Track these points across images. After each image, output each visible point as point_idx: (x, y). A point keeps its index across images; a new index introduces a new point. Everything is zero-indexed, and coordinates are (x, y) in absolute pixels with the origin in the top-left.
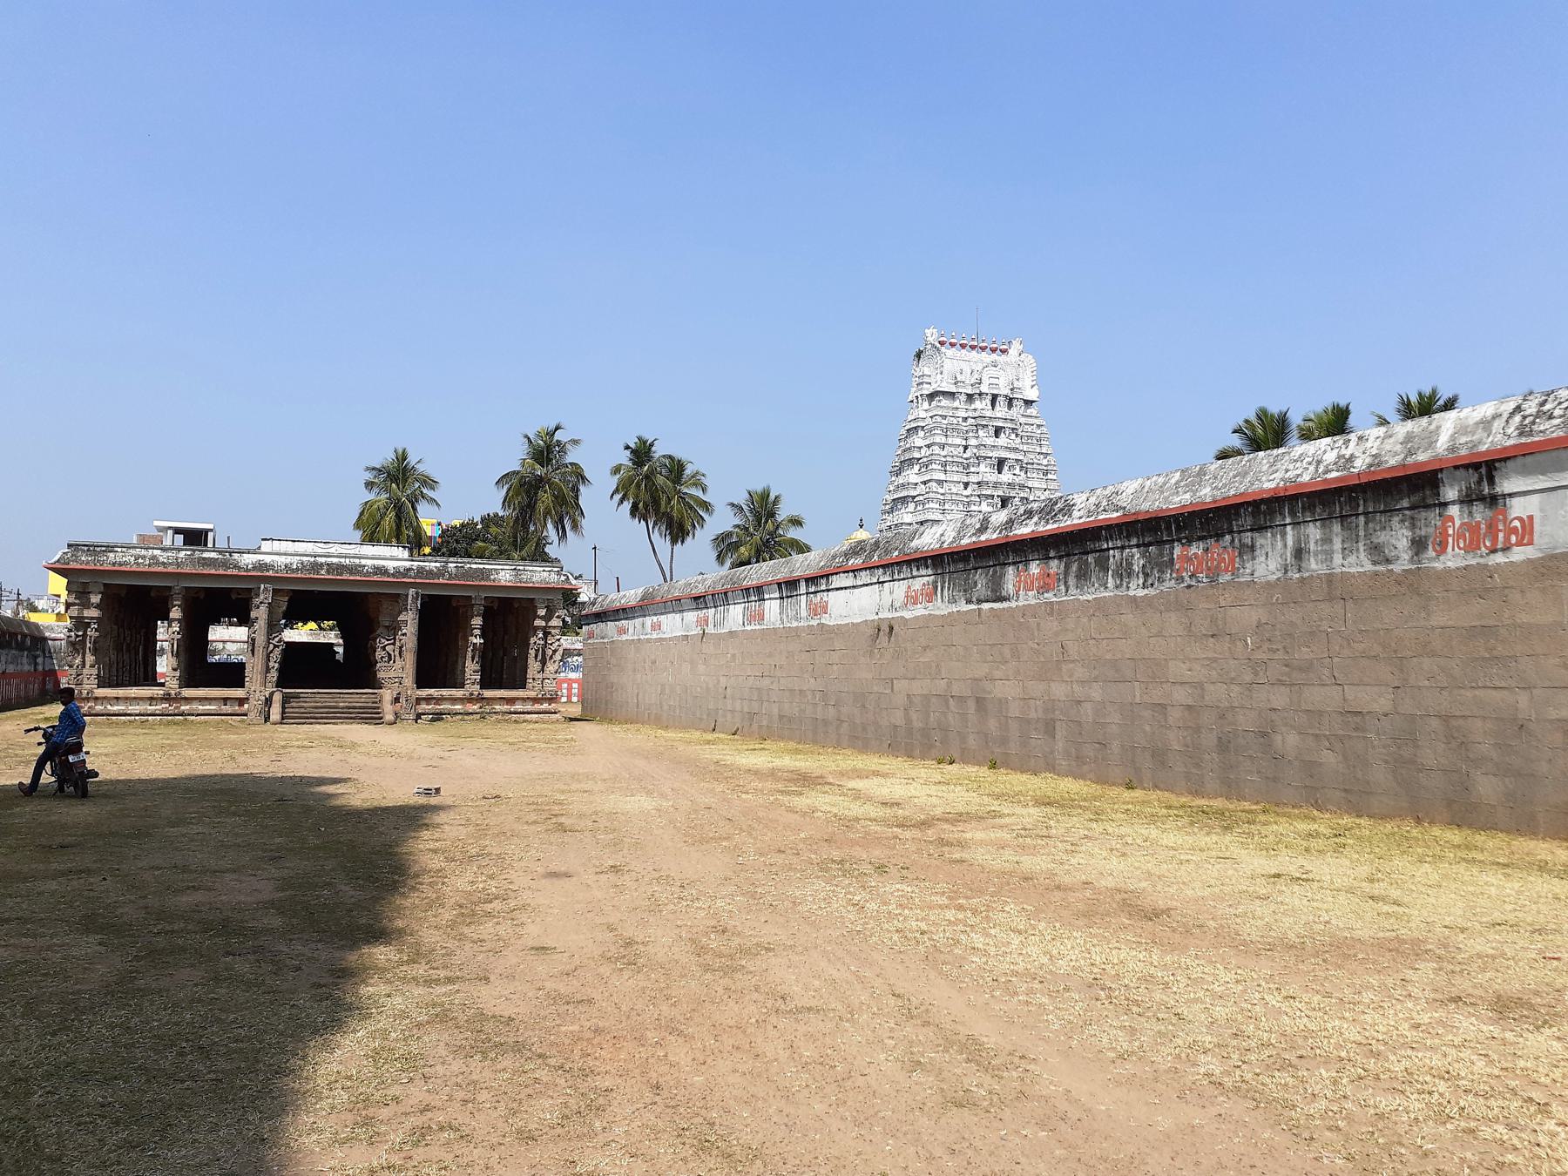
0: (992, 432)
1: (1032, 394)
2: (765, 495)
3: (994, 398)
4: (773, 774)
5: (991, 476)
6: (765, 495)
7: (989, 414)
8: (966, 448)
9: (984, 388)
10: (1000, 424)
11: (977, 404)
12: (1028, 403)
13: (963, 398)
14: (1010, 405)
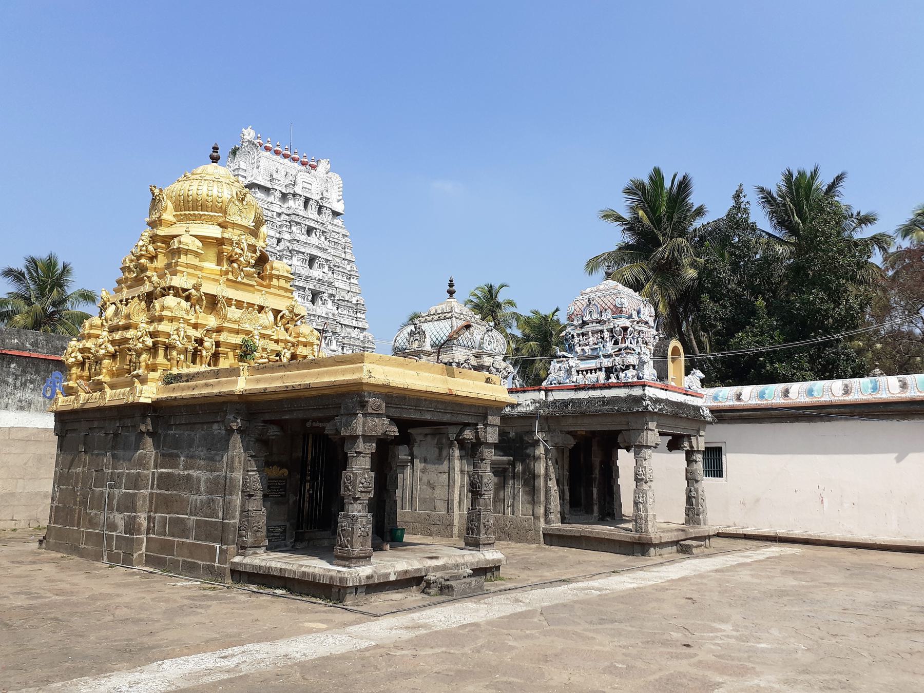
0: (304, 230)
1: (339, 207)
2: (50, 264)
3: (307, 201)
6: (50, 264)
7: (301, 213)
8: (279, 241)
9: (298, 190)
10: (312, 224)
11: (291, 203)
12: (336, 214)
13: (278, 195)
14: (320, 212)
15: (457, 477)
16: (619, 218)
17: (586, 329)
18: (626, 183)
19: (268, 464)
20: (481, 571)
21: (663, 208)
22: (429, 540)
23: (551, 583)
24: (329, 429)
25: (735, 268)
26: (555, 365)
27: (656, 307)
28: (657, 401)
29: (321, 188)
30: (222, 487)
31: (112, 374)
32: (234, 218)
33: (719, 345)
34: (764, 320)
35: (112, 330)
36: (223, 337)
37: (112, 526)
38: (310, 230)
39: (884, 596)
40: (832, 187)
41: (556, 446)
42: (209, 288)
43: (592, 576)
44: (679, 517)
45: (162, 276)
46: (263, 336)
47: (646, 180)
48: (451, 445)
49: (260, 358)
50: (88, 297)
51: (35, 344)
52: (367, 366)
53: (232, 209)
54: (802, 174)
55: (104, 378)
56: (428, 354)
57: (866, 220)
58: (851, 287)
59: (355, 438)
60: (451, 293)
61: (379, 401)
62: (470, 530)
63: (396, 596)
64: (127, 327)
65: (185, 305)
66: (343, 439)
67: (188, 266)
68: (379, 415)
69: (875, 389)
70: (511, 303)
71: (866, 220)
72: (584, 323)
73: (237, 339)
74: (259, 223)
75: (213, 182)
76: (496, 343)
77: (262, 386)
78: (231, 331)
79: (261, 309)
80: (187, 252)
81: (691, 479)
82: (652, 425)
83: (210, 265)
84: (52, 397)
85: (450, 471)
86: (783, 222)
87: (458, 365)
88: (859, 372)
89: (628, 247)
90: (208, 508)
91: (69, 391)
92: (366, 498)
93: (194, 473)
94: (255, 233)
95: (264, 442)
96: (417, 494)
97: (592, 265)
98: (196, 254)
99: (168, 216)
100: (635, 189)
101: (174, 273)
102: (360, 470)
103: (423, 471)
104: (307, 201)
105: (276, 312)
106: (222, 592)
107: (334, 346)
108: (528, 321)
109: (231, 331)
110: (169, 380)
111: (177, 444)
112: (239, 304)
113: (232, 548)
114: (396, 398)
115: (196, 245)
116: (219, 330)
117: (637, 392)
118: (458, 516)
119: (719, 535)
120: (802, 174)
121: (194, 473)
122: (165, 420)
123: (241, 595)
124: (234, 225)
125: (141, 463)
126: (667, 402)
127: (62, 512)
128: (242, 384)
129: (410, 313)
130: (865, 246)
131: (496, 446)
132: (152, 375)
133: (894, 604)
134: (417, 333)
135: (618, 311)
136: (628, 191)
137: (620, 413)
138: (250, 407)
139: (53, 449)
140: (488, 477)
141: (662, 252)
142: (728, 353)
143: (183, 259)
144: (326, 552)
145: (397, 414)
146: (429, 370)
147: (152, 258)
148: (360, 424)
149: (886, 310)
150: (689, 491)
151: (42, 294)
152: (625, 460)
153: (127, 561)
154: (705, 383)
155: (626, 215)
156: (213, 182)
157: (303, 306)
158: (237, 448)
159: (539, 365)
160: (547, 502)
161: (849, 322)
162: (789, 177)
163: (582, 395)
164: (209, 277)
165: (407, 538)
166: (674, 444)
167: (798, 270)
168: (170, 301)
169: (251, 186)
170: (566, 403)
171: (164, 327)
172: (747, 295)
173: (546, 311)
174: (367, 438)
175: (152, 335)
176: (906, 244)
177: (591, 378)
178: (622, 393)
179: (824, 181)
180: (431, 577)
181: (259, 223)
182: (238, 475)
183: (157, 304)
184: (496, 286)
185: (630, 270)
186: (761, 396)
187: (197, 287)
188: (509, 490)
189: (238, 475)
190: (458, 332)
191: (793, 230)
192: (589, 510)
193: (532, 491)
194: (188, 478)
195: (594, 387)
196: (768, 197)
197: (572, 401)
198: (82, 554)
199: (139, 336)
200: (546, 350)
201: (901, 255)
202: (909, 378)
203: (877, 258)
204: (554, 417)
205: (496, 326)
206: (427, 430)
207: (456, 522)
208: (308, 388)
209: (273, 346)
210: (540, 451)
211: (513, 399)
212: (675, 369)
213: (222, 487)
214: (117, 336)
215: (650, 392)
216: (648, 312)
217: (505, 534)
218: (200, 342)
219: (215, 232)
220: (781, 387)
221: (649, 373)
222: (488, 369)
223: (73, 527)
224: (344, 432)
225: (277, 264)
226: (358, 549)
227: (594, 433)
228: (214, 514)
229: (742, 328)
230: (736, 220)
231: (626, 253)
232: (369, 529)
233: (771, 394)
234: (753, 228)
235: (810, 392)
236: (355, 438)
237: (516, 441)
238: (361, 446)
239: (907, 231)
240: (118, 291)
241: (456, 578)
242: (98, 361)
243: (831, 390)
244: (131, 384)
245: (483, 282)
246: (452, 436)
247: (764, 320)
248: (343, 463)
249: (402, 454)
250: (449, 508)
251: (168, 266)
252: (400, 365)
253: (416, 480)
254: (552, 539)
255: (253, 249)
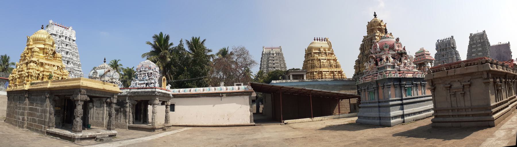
1: (75, 39)
2: (5, 56)
4: (340, 86)
5: (65, 55)
6: (5, 56)
9: (64, 35)
11: (62, 38)
12: (74, 40)
15: (105, 111)
16: (151, 44)
17: (141, 73)
18: (153, 35)
19: (55, 106)
20: (111, 136)
21: (162, 42)
22: (97, 128)
23: (130, 139)
24: (71, 98)
25: (180, 59)
26: (132, 82)
27: (160, 67)
28: (159, 92)
29: (70, 34)
30: (44, 111)
31: (19, 82)
32: (48, 43)
33: (175, 78)
34: (186, 73)
35: (19, 72)
36: (44, 73)
37: (19, 119)
38: (67, 45)
39: (209, 137)
40: (203, 42)
41: (132, 104)
42: (41, 61)
43: (140, 137)
44: (163, 121)
45: (30, 58)
46: (54, 73)
47: (158, 35)
48: (104, 103)
49: (54, 79)
50: (13, 64)
51: (3, 75)
52: (81, 81)
53: (47, 40)
54: (196, 38)
55: (17, 83)
56: (98, 78)
57: (210, 51)
58: (206, 66)
59: (78, 100)
60: (105, 62)
61: (84, 91)
62: (108, 125)
63: (88, 141)
64: (22, 71)
65: (35, 65)
66: (75, 101)
67: (36, 55)
68: (85, 95)
69: (209, 90)
70: (121, 65)
71: (210, 51)
72: (141, 71)
73: (48, 74)
74: (53, 43)
75: (42, 34)
76: (117, 76)
77: (54, 86)
78: (47, 72)
79: (54, 66)
80: (36, 52)
81: (167, 112)
82: (157, 99)
83: (41, 55)
84: (6, 88)
85: (103, 110)
86: (191, 49)
87: (106, 81)
88: (207, 86)
89: (153, 51)
90: (41, 116)
91: (10, 87)
92: (81, 116)
93: (38, 108)
94: (52, 46)
95: (55, 101)
96: (94, 116)
97: (143, 56)
98: (38, 52)
99: (31, 43)
100: (155, 37)
101: (33, 57)
102: (79, 109)
103: (96, 110)
104: (66, 37)
105: (58, 67)
106: (44, 137)
107: (73, 76)
108: (125, 70)
109: (47, 72)
110: (32, 84)
111: (33, 100)
112: (48, 65)
113: (47, 127)
114: (89, 90)
115: (38, 50)
116: (43, 71)
117: (154, 90)
118: (105, 122)
119: (173, 126)
120: (196, 38)
121: (38, 108)
122: (33, 95)
123: (49, 138)
124: (47, 44)
125: (25, 104)
126: (162, 93)
127: (8, 115)
128: (49, 85)
129: (94, 67)
130: (209, 57)
131: (116, 104)
132: (28, 83)
133: (210, 139)
134: (95, 73)
135: (150, 68)
136: (154, 37)
137: (149, 95)
138: (51, 91)
139: (7, 100)
140: (114, 112)
141: (162, 53)
142: (177, 80)
143: (35, 54)
144: (70, 129)
145: (89, 94)
146: (98, 82)
147: (28, 54)
148: (79, 97)
149: (213, 72)
150: (166, 115)
151: (4, 64)
152: (150, 107)
153: (23, 127)
154: (171, 88)
155: (153, 43)
156: (42, 34)
157: (64, 65)
158: (48, 102)
159: (128, 82)
160: (129, 119)
161: (205, 74)
162: (193, 38)
163: (139, 90)
164: (40, 57)
165: (91, 127)
166: (163, 104)
167: (194, 61)
168: (32, 64)
169: (51, 34)
170: (135, 92)
171: (30, 71)
172: (182, 66)
173: (131, 67)
174: (81, 101)
175: (28, 73)
176: (217, 57)
177: (142, 86)
178: (150, 90)
179: (201, 40)
180: (98, 137)
181: (53, 43)
182: (48, 109)
183: (29, 65)
184: (117, 60)
185: (153, 58)
186: (185, 91)
187: (38, 61)
188: (119, 115)
189: (48, 109)
190: (106, 72)
191: (194, 51)
192: (140, 121)
193: (125, 116)
194: (36, 109)
195: (143, 88)
196: (188, 42)
197: (137, 92)
198: (13, 124)
199: (25, 73)
200: (130, 78)
201: (216, 60)
202: (216, 88)
203: (211, 60)
204: (132, 96)
205: (117, 71)
206: (97, 99)
207: (105, 123)
208: (66, 87)
209: (57, 75)
210: (128, 105)
211: (121, 91)
212: (164, 84)
213: (44, 111)
214: (20, 73)
215: (157, 90)
216: (157, 69)
217: (117, 127)
218: (39, 74)
219: (42, 46)
220: (189, 89)
221: (157, 85)
222: (114, 83)
223: (11, 118)
224: (75, 99)
225: (58, 54)
226: (78, 129)
227: (142, 100)
228: (42, 118)
229: (181, 74)
230: (180, 47)
231: (152, 53)
232: (81, 124)
233: (187, 91)
234: (184, 50)
235: (196, 91)
236: (78, 100)
237: (121, 102)
238: (79, 102)
239: (217, 54)
240: (20, 62)
241: (105, 137)
242: (16, 79)
243: (200, 90)
244: (23, 85)
245: (114, 59)
246: (104, 101)
247: (186, 73)
248: (75, 107)
249: (91, 105)
250: (103, 120)
251: (31, 55)
252: (90, 81)
253: (94, 112)
254: (130, 128)
255: (52, 50)
